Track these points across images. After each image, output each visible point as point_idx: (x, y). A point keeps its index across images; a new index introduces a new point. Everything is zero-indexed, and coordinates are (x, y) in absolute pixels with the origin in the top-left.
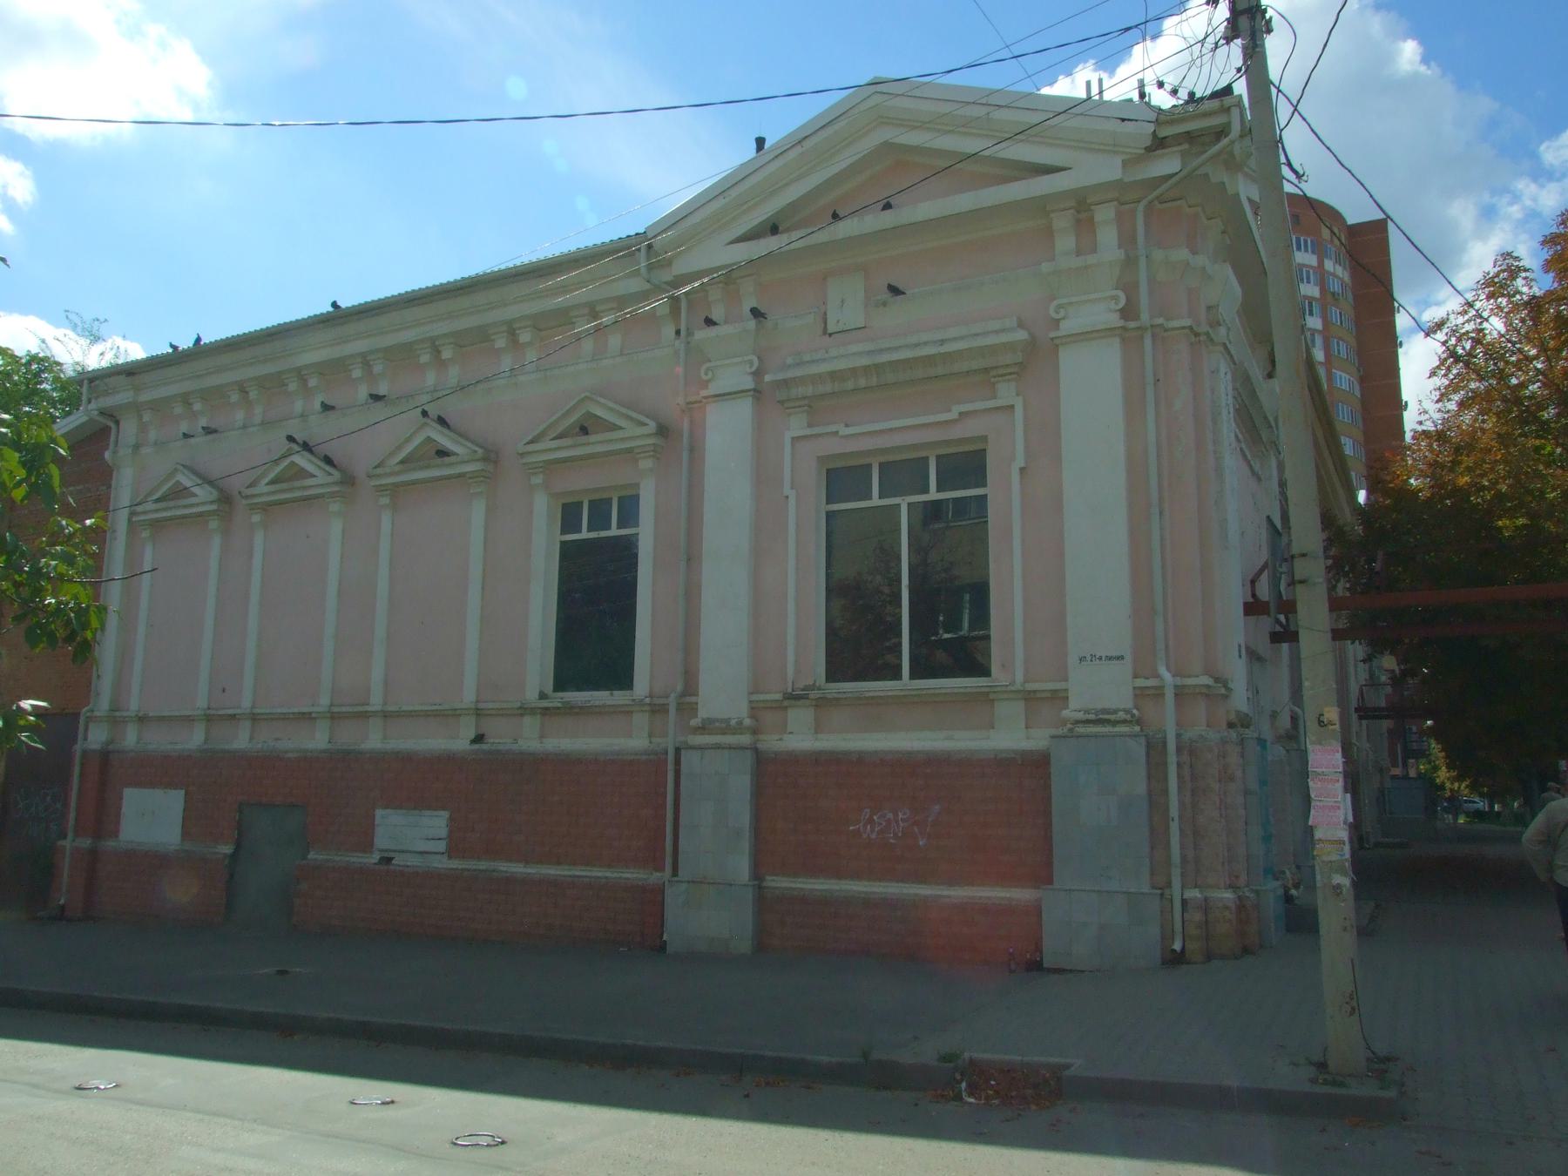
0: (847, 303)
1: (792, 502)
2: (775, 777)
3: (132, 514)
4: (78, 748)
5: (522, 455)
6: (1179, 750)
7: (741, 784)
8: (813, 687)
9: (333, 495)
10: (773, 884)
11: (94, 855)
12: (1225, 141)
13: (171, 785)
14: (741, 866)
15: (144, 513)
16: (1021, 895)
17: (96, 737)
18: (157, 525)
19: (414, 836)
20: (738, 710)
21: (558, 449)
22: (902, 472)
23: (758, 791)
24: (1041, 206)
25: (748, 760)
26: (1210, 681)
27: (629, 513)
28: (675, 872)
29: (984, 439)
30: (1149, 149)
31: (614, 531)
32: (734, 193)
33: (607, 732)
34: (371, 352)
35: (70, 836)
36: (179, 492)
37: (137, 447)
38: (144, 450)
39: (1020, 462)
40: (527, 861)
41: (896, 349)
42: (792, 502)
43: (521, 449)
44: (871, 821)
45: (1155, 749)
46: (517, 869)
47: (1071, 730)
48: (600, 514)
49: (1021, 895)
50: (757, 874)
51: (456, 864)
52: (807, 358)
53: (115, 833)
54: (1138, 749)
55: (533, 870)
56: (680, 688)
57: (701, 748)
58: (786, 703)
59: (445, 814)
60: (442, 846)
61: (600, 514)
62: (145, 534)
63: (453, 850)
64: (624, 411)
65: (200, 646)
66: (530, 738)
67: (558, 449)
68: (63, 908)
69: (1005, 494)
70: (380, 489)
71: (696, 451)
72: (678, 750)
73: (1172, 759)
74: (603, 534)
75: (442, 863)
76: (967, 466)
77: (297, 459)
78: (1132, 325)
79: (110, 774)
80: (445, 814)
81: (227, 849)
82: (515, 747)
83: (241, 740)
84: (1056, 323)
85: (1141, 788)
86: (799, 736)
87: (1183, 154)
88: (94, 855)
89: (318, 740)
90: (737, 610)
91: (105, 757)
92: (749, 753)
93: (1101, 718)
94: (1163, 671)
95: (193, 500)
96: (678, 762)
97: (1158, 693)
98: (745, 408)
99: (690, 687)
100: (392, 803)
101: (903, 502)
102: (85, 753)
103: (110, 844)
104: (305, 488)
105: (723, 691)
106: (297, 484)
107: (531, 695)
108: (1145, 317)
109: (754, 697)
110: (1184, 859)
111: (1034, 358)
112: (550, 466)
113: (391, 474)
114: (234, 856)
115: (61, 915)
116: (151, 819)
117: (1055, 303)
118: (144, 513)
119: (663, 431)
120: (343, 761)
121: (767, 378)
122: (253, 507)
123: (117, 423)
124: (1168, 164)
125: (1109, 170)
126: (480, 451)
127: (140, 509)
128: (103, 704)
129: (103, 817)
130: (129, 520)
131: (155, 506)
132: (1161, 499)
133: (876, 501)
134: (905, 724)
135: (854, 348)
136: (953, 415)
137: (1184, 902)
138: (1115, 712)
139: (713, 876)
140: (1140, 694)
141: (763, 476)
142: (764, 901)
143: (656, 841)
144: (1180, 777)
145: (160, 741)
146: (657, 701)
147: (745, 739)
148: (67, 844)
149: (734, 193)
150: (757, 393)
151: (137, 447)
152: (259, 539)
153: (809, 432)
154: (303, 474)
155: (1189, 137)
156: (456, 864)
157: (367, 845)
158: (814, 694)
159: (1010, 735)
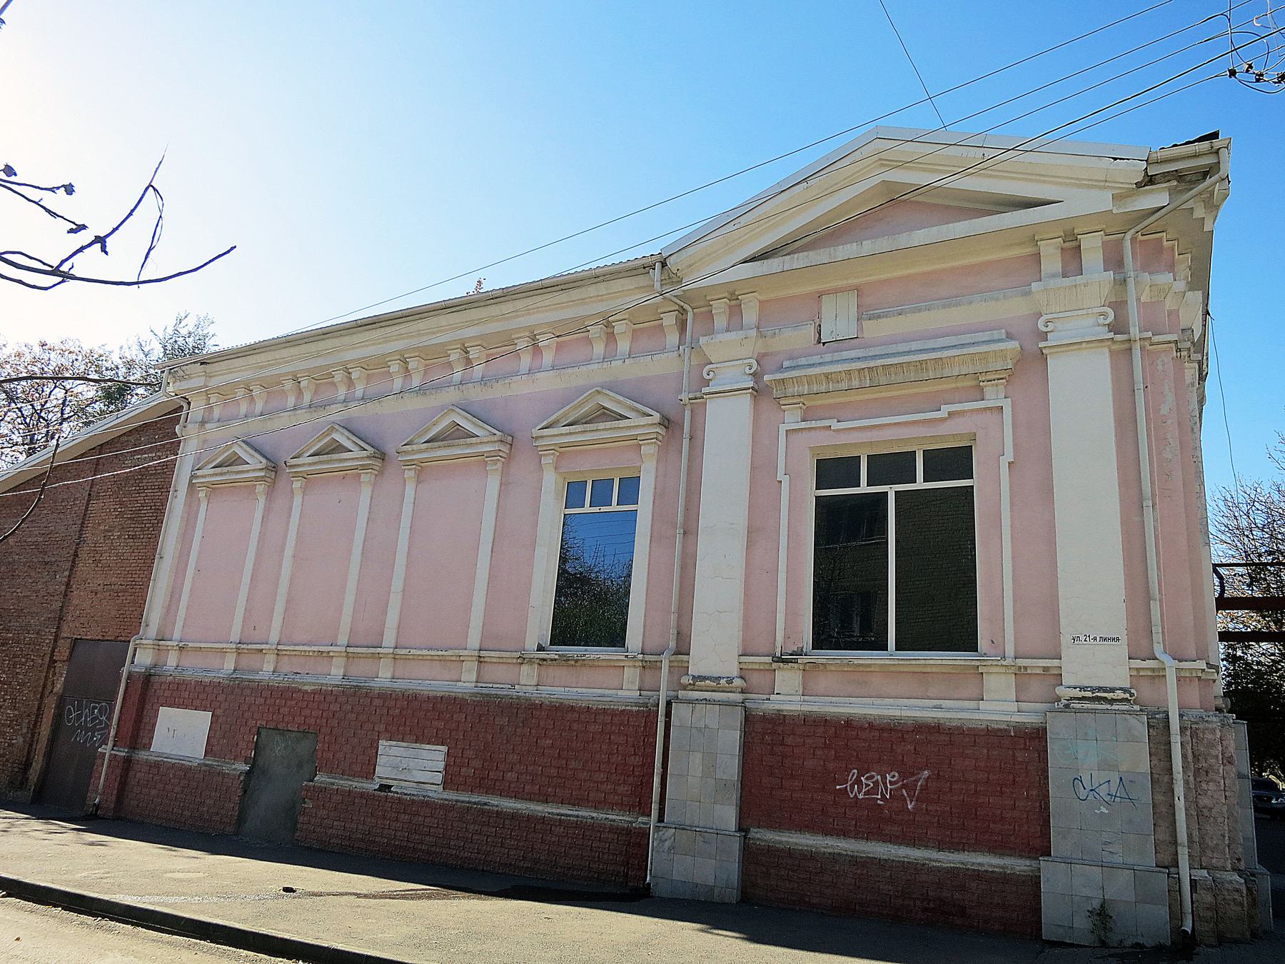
0: (839, 319)
1: (785, 485)
2: (767, 739)
3: (193, 477)
4: (125, 671)
5: (537, 438)
6: (1183, 730)
7: (731, 738)
8: (800, 653)
9: (364, 467)
10: (758, 836)
11: (128, 761)
12: (1209, 181)
14: (728, 816)
15: (203, 477)
16: (1018, 865)
17: (143, 658)
18: (213, 488)
19: (414, 767)
20: (727, 665)
21: (314, 464)
22: (892, 466)
23: (746, 747)
24: (1032, 237)
25: (739, 714)
27: (630, 488)
28: (661, 818)
30: (1139, 185)
33: (604, 680)
34: (407, 350)
36: (235, 461)
37: (203, 423)
38: (208, 426)
39: (1009, 455)
40: (516, 796)
42: (785, 485)
43: (536, 432)
44: (858, 782)
45: (1159, 726)
46: (508, 804)
47: (1067, 706)
48: (602, 491)
49: (1018, 865)
50: (742, 828)
51: (451, 796)
52: (803, 361)
54: (1140, 727)
56: (672, 644)
57: (690, 702)
58: (775, 665)
59: (444, 749)
60: (439, 778)
61: (602, 495)
62: (202, 495)
63: (446, 784)
64: (629, 402)
65: (229, 596)
66: (528, 683)
67: (314, 464)
68: (97, 807)
69: (991, 488)
70: (410, 463)
71: (696, 439)
72: (669, 704)
73: (1176, 739)
74: (604, 509)
75: (437, 793)
76: (954, 461)
77: (337, 436)
78: (1119, 337)
79: (149, 693)
80: (444, 749)
82: (513, 693)
83: (266, 670)
84: (1044, 336)
85: (1145, 767)
86: (788, 695)
87: (1172, 192)
89: (335, 674)
90: (730, 599)
92: (739, 710)
93: (1098, 696)
94: (1158, 649)
95: (246, 467)
96: (668, 714)
97: (1158, 676)
98: (745, 401)
99: (682, 649)
100: (397, 734)
101: (891, 490)
103: (142, 755)
104: (238, 472)
105: (715, 651)
106: (335, 456)
107: (531, 644)
108: (1135, 332)
109: (744, 659)
110: (1190, 836)
111: (1032, 361)
112: (562, 452)
113: (420, 451)
114: (248, 773)
116: (181, 734)
117: (1045, 317)
118: (203, 477)
119: (666, 422)
121: (766, 378)
122: (296, 475)
123: (189, 403)
124: (1158, 198)
125: (1102, 202)
126: (264, 461)
127: (199, 473)
128: (152, 631)
129: (138, 730)
130: (190, 481)
132: (1153, 495)
133: (864, 488)
134: (889, 687)
135: (846, 355)
136: (943, 413)
137: (1193, 883)
138: (1112, 690)
139: (701, 782)
140: (1137, 675)
141: (761, 469)
142: (750, 854)
144: (1184, 756)
145: (196, 667)
146: (648, 658)
147: (738, 697)
148: (106, 750)
150: (758, 392)
151: (203, 423)
152: (298, 500)
153: (803, 425)
154: (340, 448)
155: (1178, 176)
156: (451, 796)
157: (369, 774)
158: (802, 659)
159: (998, 703)
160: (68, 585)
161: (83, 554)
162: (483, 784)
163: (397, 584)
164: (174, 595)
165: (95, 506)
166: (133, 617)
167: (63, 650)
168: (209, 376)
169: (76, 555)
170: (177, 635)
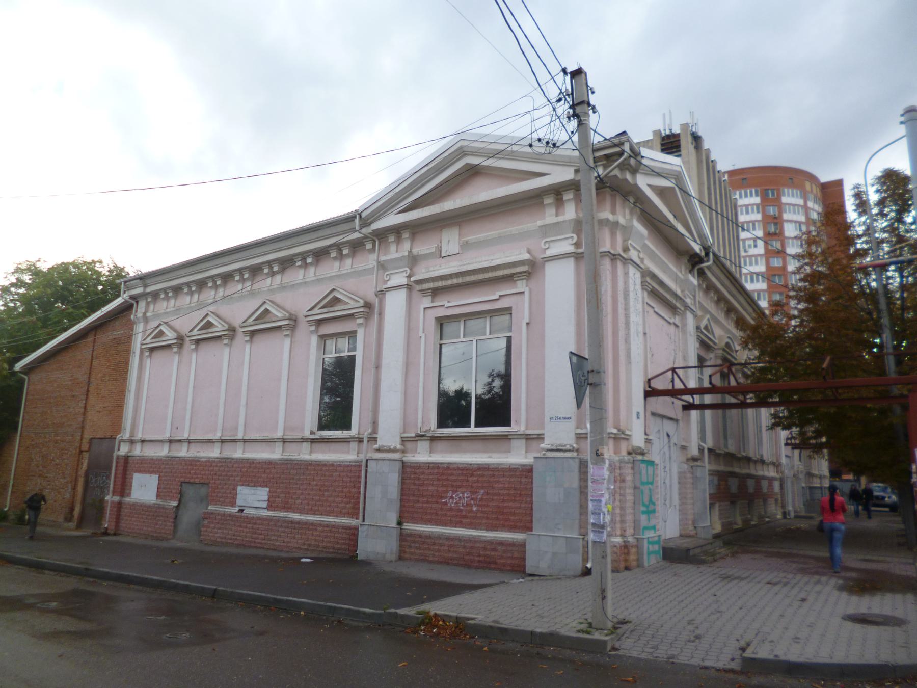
11: (119, 505)
18: (152, 350)
53: (129, 495)
60: (265, 505)
63: (270, 507)
68: (106, 529)
81: (175, 504)
88: (119, 505)
89: (214, 452)
102: (118, 457)
114: (177, 507)
116: (144, 489)
129: (124, 488)
160: (85, 408)
162: (287, 507)
166: (117, 424)
167: (85, 447)
168: (145, 286)
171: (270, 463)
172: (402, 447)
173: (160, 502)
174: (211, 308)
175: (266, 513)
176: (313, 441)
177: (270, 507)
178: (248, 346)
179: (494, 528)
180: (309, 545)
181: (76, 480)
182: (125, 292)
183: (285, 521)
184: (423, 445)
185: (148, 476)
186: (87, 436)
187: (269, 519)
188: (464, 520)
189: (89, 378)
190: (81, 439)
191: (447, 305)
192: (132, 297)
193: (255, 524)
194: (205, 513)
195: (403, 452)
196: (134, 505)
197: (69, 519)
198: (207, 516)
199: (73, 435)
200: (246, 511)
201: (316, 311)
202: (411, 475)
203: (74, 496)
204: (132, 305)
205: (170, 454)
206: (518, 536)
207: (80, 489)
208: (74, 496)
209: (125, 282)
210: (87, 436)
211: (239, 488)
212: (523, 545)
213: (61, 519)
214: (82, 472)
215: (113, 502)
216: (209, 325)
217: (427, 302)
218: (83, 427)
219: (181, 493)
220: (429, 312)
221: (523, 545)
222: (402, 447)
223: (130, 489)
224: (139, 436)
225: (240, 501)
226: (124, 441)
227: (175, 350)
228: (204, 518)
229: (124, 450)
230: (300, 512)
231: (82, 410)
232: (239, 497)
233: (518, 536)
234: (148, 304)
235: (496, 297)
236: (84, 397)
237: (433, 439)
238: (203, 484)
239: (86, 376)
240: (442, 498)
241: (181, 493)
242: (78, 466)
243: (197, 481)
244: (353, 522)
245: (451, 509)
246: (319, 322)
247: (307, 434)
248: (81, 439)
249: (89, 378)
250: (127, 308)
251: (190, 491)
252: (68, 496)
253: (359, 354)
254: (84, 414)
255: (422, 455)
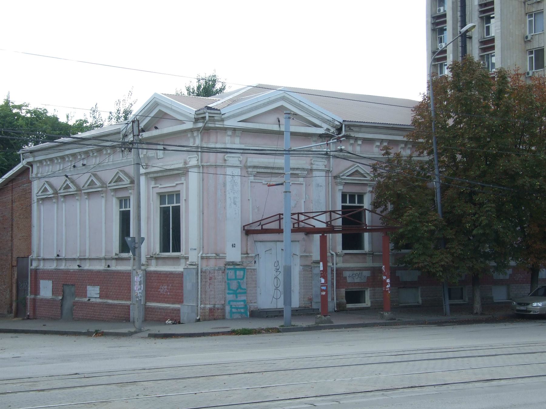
6: (201, 272)
11: (34, 300)
13: (49, 279)
18: (43, 199)
26: (215, 255)
29: (179, 191)
31: (356, 204)
32: (146, 109)
35: (29, 294)
41: (265, 150)
48: (352, 197)
53: (39, 294)
55: (116, 302)
60: (98, 296)
61: (352, 200)
63: (100, 297)
68: (29, 316)
81: (60, 298)
88: (34, 300)
89: (74, 266)
91: (36, 271)
102: (31, 270)
103: (38, 297)
114: (62, 299)
115: (28, 318)
116: (46, 290)
120: (81, 272)
129: (36, 290)
131: (115, 184)
143: (127, 293)
149: (146, 109)
160: (12, 237)
161: (14, 224)
162: (107, 297)
163: (87, 235)
164: (39, 245)
165: (14, 205)
166: (29, 249)
167: (15, 263)
168: (34, 157)
169: (12, 225)
170: (42, 256)
171: (99, 272)
172: (146, 263)
173: (54, 297)
174: (47, 180)
175: (99, 300)
176: (116, 259)
177: (100, 297)
178: (87, 201)
179: (173, 303)
180: (115, 316)
181: (12, 284)
182: (23, 159)
183: (106, 305)
184: (153, 262)
185: (47, 281)
186: (15, 256)
187: (100, 304)
188: (166, 300)
189: (12, 216)
190: (12, 258)
191: (160, 186)
192: (29, 163)
193: (95, 307)
194: (74, 302)
195: (148, 265)
196: (42, 299)
197: (10, 312)
198: (75, 304)
199: (7, 256)
200: (92, 300)
201: (112, 184)
202: (149, 277)
203: (11, 297)
204: (29, 168)
205: (58, 268)
206: (177, 306)
207: (14, 291)
208: (11, 297)
209: (23, 154)
210: (15, 256)
211: (88, 287)
212: (178, 310)
213: (6, 313)
214: (14, 280)
215: (31, 298)
216: (119, 180)
217: (153, 184)
218: (12, 250)
219: (63, 291)
220: (154, 189)
221: (178, 310)
222: (146, 263)
223: (39, 290)
224: (42, 256)
225: (88, 295)
226: (35, 259)
227: (54, 201)
228: (74, 305)
229: (35, 264)
230: (113, 299)
231: (10, 238)
232: (88, 292)
233: (177, 306)
234: (38, 167)
235: (175, 185)
236: (10, 229)
237: (157, 259)
238: (72, 285)
239: (10, 214)
240: (159, 289)
241: (63, 291)
242: (12, 276)
243: (69, 283)
244: (128, 303)
245: (161, 294)
246: (116, 190)
247: (114, 255)
248: (12, 258)
249: (12, 216)
250: (25, 171)
251: (67, 290)
252: (8, 296)
253: (131, 209)
254: (12, 241)
255: (153, 268)
